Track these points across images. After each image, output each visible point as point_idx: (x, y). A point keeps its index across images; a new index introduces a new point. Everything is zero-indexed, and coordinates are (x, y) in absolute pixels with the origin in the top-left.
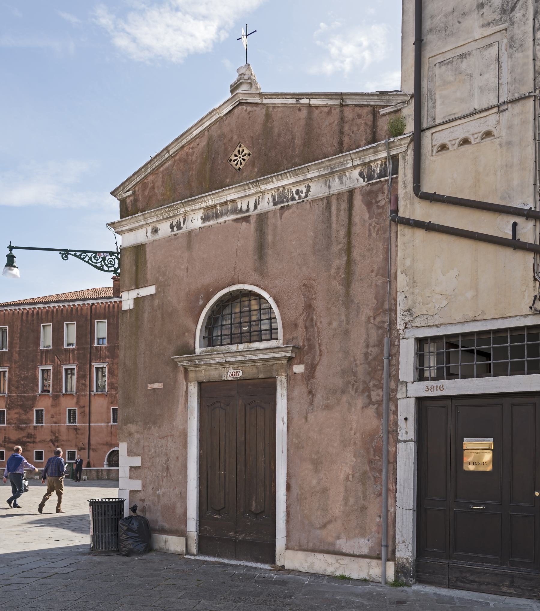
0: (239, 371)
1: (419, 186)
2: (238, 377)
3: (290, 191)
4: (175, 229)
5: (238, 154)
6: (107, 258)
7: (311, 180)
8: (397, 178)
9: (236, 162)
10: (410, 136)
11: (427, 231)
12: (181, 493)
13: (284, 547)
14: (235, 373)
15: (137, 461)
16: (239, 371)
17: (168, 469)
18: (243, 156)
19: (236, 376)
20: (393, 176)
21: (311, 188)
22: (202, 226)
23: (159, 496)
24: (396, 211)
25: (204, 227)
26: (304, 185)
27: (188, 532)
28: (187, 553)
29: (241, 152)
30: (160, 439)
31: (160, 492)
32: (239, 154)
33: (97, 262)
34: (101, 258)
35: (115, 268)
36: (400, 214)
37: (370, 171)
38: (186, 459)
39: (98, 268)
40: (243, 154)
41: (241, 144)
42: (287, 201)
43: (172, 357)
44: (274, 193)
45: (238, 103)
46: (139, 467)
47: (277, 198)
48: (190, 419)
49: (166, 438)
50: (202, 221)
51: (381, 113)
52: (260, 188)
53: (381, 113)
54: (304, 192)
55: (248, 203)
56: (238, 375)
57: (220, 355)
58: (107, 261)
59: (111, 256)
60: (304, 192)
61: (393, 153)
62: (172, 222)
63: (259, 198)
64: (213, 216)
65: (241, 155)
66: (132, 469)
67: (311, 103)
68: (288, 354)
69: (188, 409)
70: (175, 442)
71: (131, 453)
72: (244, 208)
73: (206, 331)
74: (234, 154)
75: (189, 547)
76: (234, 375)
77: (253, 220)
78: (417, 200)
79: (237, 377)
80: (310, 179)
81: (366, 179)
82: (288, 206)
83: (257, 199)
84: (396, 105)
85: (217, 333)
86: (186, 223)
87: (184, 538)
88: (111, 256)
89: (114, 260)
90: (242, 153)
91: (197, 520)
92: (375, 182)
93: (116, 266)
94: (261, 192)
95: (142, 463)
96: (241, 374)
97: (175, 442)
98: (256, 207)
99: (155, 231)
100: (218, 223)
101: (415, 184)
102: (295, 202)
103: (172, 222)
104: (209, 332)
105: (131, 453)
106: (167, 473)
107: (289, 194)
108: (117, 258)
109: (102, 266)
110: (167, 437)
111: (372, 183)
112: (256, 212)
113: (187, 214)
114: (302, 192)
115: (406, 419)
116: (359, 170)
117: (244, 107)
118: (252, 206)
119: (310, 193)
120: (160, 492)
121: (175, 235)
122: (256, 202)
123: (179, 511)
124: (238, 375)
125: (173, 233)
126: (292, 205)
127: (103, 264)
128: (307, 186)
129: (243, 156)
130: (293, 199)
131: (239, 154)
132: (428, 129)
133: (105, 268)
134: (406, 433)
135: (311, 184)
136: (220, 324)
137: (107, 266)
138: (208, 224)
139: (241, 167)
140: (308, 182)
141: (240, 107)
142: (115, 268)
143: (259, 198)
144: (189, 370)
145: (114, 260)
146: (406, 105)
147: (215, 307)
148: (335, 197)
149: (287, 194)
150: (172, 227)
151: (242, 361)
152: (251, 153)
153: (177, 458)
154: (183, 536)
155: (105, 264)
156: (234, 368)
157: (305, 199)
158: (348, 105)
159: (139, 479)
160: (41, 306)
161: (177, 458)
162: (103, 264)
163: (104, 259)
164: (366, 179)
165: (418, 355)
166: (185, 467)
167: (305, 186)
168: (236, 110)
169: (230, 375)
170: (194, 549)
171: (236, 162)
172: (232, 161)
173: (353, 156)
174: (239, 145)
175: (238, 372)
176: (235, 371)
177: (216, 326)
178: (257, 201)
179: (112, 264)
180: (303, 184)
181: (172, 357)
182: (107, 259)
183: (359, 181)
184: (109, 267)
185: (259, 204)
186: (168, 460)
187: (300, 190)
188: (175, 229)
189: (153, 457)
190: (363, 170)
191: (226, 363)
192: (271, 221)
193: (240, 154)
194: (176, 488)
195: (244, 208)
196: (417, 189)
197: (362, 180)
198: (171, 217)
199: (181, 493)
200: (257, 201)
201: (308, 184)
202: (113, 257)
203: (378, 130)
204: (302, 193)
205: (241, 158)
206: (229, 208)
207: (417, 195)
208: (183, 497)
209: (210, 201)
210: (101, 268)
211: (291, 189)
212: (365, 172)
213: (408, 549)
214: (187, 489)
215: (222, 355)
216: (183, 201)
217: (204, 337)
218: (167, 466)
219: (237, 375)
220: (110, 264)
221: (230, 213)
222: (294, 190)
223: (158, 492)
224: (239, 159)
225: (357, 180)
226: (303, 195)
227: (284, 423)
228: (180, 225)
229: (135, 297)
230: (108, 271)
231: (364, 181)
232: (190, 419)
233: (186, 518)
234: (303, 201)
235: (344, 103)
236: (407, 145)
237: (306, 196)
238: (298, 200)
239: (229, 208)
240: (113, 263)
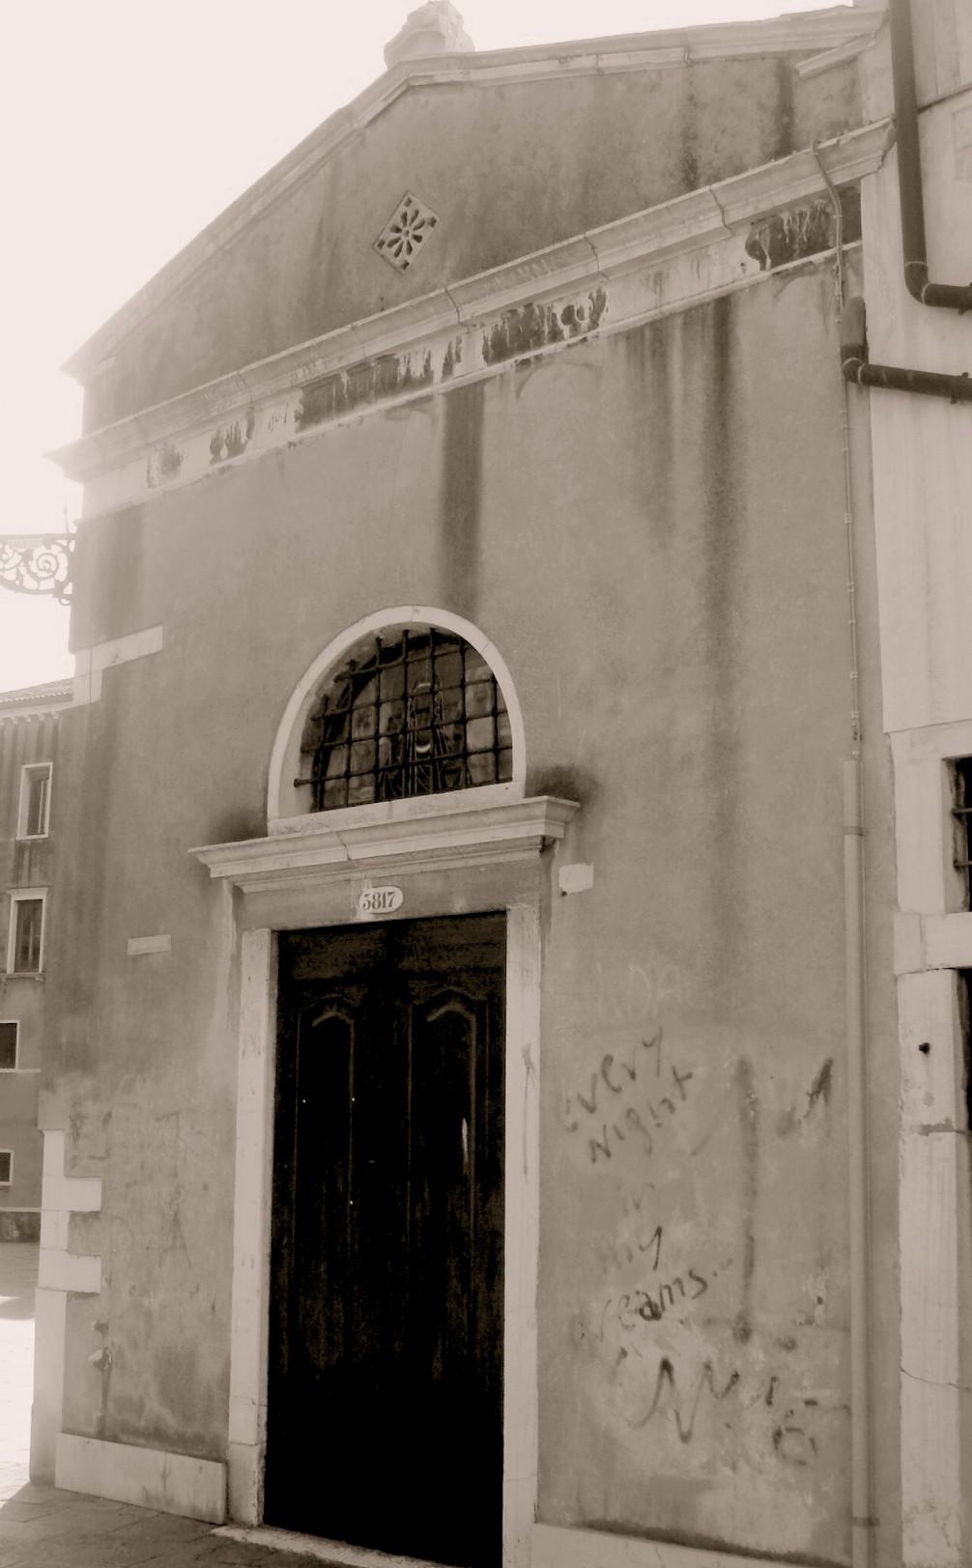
0: (391, 889)
1: (924, 270)
2: (390, 909)
3: (546, 314)
4: (224, 452)
5: (401, 226)
6: (36, 553)
7: (604, 275)
8: (858, 250)
9: (396, 247)
10: (884, 127)
11: (959, 402)
12: (213, 1308)
13: (533, 1518)
14: (381, 899)
15: (88, 1195)
16: (391, 889)
17: (176, 1221)
18: (415, 229)
19: (384, 906)
20: (846, 247)
21: (607, 301)
22: (296, 437)
23: (148, 1315)
24: (862, 350)
25: (301, 442)
26: (588, 295)
27: (233, 1443)
28: (230, 1519)
29: (409, 217)
30: (158, 1120)
31: (153, 1302)
32: (405, 224)
33: (7, 566)
34: (19, 554)
35: (56, 581)
36: (875, 358)
37: (780, 236)
38: (229, 1192)
39: (10, 585)
40: (416, 223)
41: (412, 197)
42: (539, 344)
43: (193, 850)
44: (500, 323)
45: (403, 88)
46: (95, 1215)
47: (511, 336)
48: (244, 1053)
49: (174, 1117)
50: (297, 424)
51: (802, 72)
52: (458, 311)
53: (802, 72)
54: (587, 314)
55: (428, 361)
56: (390, 905)
57: (326, 840)
58: (35, 562)
59: (49, 548)
60: (587, 314)
61: (840, 178)
62: (219, 432)
63: (459, 341)
64: (330, 407)
65: (410, 225)
66: (82, 1219)
67: (601, 65)
68: (539, 829)
69: (242, 1021)
70: (199, 1133)
71: (74, 1167)
72: (417, 370)
73: (302, 760)
74: (390, 225)
75: (234, 1495)
76: (376, 905)
77: (440, 407)
78: (924, 312)
79: (387, 909)
80: (603, 274)
81: (769, 261)
82: (538, 358)
83: (454, 345)
84: (844, 44)
85: (336, 766)
86: (254, 434)
87: (219, 1466)
88: (49, 548)
89: (55, 557)
90: (413, 220)
91: (260, 1405)
92: (796, 268)
93: (62, 575)
94: (462, 324)
95: (104, 1202)
96: (398, 899)
97: (199, 1133)
98: (448, 368)
99: (172, 463)
100: (340, 425)
101: (909, 263)
102: (560, 346)
103: (219, 432)
104: (315, 764)
105: (74, 1167)
106: (175, 1237)
107: (542, 322)
108: (65, 550)
109: (20, 577)
110: (176, 1114)
111: (786, 270)
112: (451, 383)
113: (256, 407)
114: (580, 312)
115: (925, 1048)
116: (747, 236)
117: (422, 98)
118: (437, 366)
119: (604, 314)
120: (153, 1302)
121: (222, 471)
122: (449, 353)
123: (207, 1370)
124: (390, 905)
125: (218, 466)
126: (552, 356)
127: (23, 570)
128: (595, 295)
129: (415, 229)
130: (556, 336)
131: (405, 224)
132: (940, 101)
133: (29, 583)
134: (929, 1100)
135: (607, 291)
136: (346, 735)
137: (34, 576)
138: (314, 430)
139: (410, 259)
140: (596, 284)
141: (409, 98)
142: (56, 581)
143: (459, 341)
144: (245, 889)
145: (55, 557)
146: (873, 43)
147: (332, 683)
148: (679, 321)
149: (538, 324)
150: (215, 449)
151: (401, 857)
152: (437, 219)
153: (206, 1188)
154: (218, 1460)
155: (29, 571)
156: (378, 882)
157: (589, 335)
158: (706, 61)
159: (95, 1256)
160: (26, 713)
161: (206, 1188)
162: (23, 570)
163: (27, 557)
164: (769, 261)
165: (964, 817)
166: (227, 1217)
167: (591, 297)
168: (400, 107)
169: (364, 905)
170: (251, 1506)
171: (396, 247)
172: (385, 246)
173: (722, 199)
174: (406, 199)
175: (390, 893)
176: (382, 890)
177: (338, 742)
178: (453, 351)
179: (49, 571)
180: (585, 291)
181: (193, 850)
182: (35, 557)
183: (747, 268)
184: (38, 580)
185: (459, 360)
186: (179, 1193)
187: (576, 309)
188: (224, 452)
189: (135, 1183)
190: (757, 236)
191: (350, 865)
192: (492, 406)
193: (408, 222)
194: (198, 1289)
195: (417, 370)
196: (917, 276)
197: (757, 264)
198: (212, 420)
199: (213, 1308)
200: (453, 351)
201: (599, 291)
202: (55, 549)
203: (797, 120)
204: (582, 319)
205: (410, 235)
206: (374, 380)
207: (916, 295)
208: (218, 1320)
209: (319, 362)
210: (18, 582)
211: (549, 309)
212: (765, 241)
213: (947, 1537)
214: (230, 1295)
215: (335, 839)
216: (242, 371)
217: (296, 780)
218: (176, 1214)
219: (387, 903)
220: (45, 570)
221: (376, 392)
222: (559, 310)
223: (146, 1302)
224: (404, 239)
225: (742, 265)
226: (585, 323)
227: (529, 1064)
228: (237, 439)
229: (108, 664)
230: (37, 592)
231: (763, 268)
232: (244, 1053)
233: (228, 1397)
234: (585, 340)
235: (693, 56)
236: (881, 153)
237: (594, 324)
238: (571, 337)
239: (374, 380)
240: (53, 569)
